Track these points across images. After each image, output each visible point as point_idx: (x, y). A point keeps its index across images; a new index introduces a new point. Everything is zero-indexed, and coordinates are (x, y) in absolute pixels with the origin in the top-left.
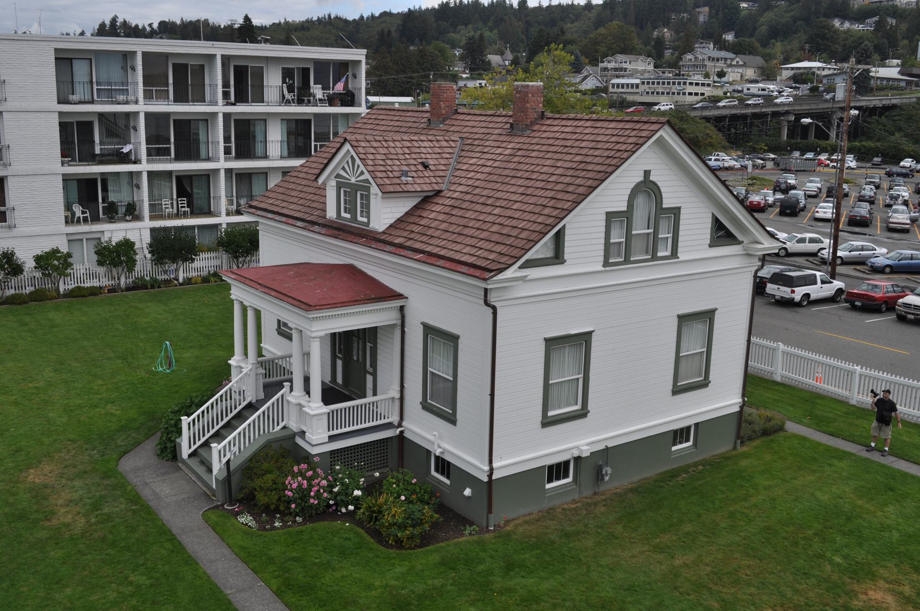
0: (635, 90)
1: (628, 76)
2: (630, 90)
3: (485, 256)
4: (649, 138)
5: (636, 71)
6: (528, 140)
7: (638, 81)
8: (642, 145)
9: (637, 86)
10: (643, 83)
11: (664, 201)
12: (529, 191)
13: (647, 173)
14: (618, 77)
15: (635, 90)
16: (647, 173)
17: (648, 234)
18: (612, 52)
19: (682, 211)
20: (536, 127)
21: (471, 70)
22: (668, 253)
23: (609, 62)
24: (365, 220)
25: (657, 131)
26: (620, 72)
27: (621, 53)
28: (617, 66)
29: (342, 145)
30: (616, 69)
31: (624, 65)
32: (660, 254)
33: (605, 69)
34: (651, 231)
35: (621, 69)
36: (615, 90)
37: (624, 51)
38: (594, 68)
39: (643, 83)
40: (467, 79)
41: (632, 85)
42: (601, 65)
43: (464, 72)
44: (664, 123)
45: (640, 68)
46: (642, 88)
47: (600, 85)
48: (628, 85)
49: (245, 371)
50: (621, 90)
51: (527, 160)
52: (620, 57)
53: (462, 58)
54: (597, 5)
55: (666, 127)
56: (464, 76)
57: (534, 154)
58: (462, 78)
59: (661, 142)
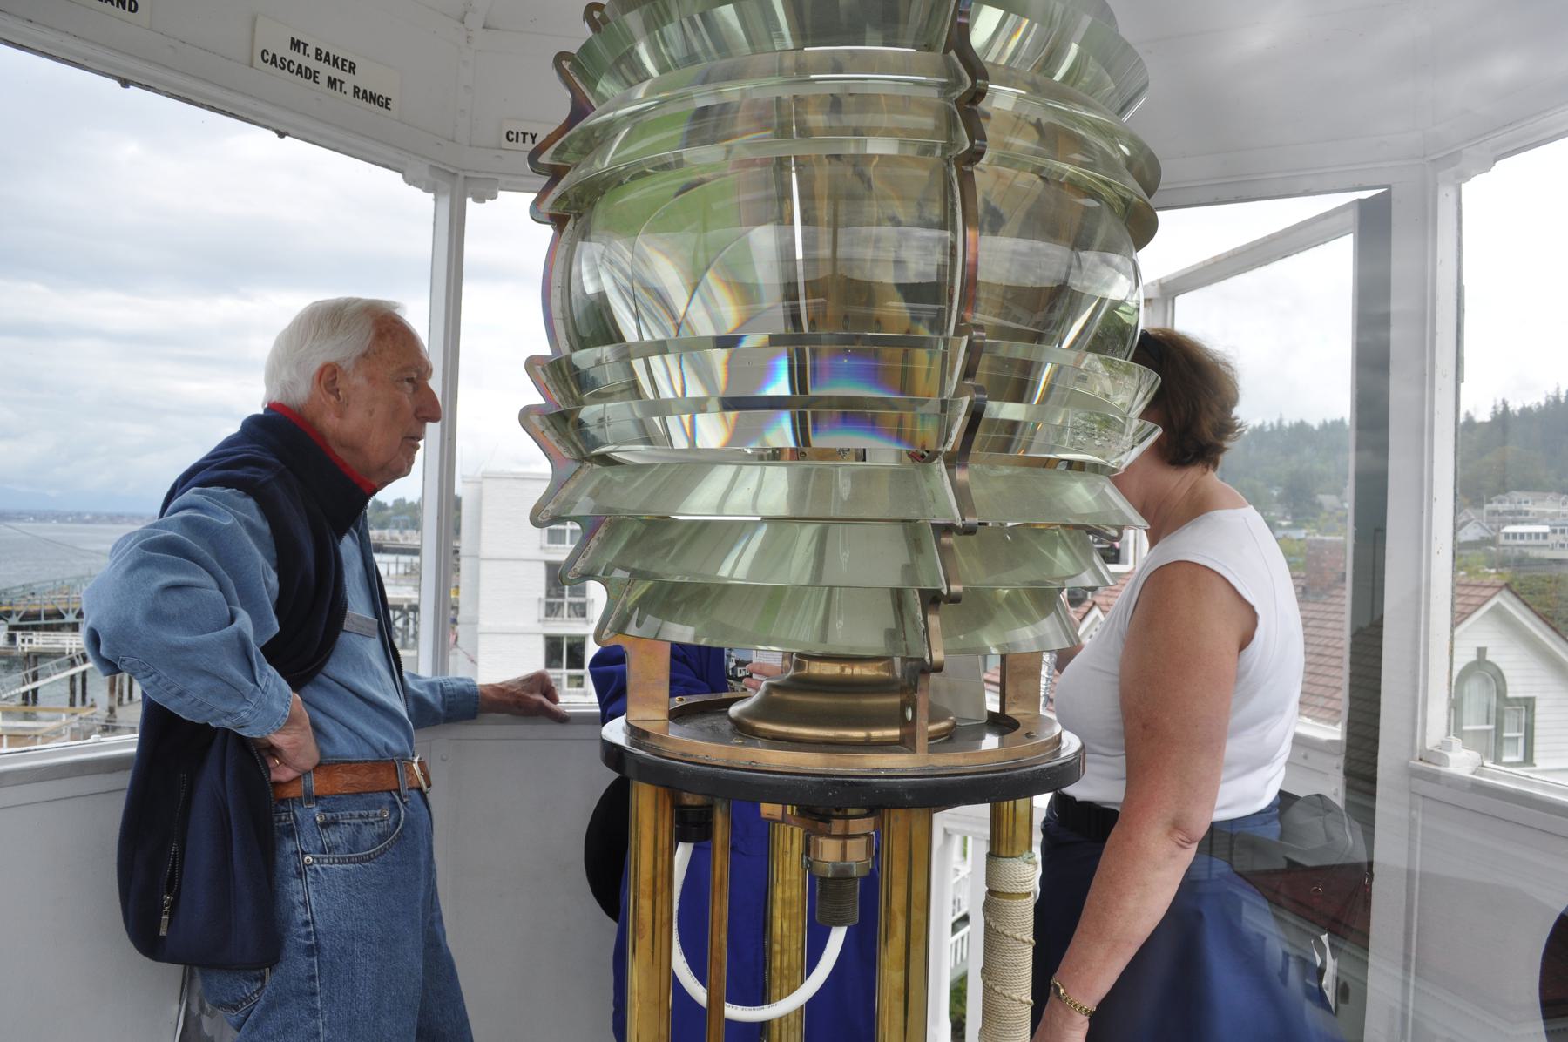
0: (1541, 541)
1: (1530, 522)
2: (1533, 541)
3: (283, 129)
4: (1479, 606)
5: (1544, 514)
6: (1323, 608)
7: (1546, 529)
8: (1470, 614)
9: (1545, 536)
10: (1554, 532)
11: (1509, 688)
12: (1320, 670)
13: (1481, 652)
14: (1515, 523)
15: (1541, 541)
16: (1481, 652)
17: (1488, 731)
18: (1503, 488)
19: (1537, 703)
20: (1335, 592)
21: (1295, 516)
22: (1519, 758)
23: (1500, 502)
24: (944, 540)
25: (1491, 597)
26: (1518, 516)
27: (1519, 489)
28: (1513, 507)
29: (1090, 609)
30: (1511, 513)
31: (1525, 507)
32: (1505, 759)
33: (1495, 512)
34: (1491, 727)
35: (1520, 512)
36: (1511, 541)
37: (1524, 486)
38: (1478, 511)
39: (1554, 532)
40: (1288, 527)
41: (1537, 535)
42: (1488, 507)
43: (1284, 518)
44: (1501, 588)
45: (1550, 510)
46: (1552, 539)
47: (1485, 534)
48: (1530, 535)
49: (962, 874)
50: (1519, 542)
51: (1321, 632)
52: (1517, 495)
53: (1280, 500)
54: (1483, 424)
55: (1505, 592)
56: (1284, 523)
57: (1330, 625)
58: (1280, 527)
59: (1498, 611)
